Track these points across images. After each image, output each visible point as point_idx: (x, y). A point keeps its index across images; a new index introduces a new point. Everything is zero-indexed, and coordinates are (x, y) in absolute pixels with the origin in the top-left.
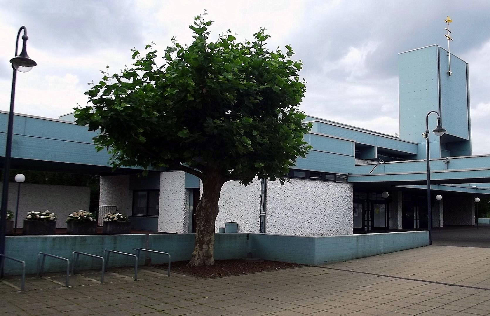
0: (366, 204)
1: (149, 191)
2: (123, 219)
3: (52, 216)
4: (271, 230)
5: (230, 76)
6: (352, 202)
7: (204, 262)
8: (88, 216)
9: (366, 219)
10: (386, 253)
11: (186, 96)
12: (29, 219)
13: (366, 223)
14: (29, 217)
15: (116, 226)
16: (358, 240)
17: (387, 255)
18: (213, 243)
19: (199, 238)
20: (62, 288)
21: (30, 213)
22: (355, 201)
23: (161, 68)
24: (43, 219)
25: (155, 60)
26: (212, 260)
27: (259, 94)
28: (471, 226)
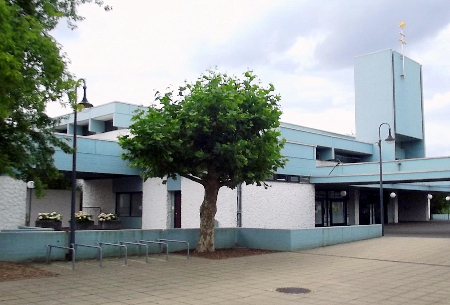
0: (325, 202)
1: (131, 194)
2: (115, 219)
3: (58, 217)
4: (245, 225)
5: (235, 113)
6: (314, 201)
7: (208, 249)
8: (87, 216)
9: (325, 216)
10: (346, 243)
11: (202, 128)
12: (41, 220)
13: (325, 220)
14: (41, 218)
15: (109, 224)
16: (323, 232)
17: (347, 244)
18: (213, 235)
19: (203, 231)
20: (123, 265)
21: (40, 214)
22: (317, 200)
23: (175, 103)
24: (51, 219)
25: (171, 98)
26: (213, 248)
27: (251, 122)
28: (426, 222)
